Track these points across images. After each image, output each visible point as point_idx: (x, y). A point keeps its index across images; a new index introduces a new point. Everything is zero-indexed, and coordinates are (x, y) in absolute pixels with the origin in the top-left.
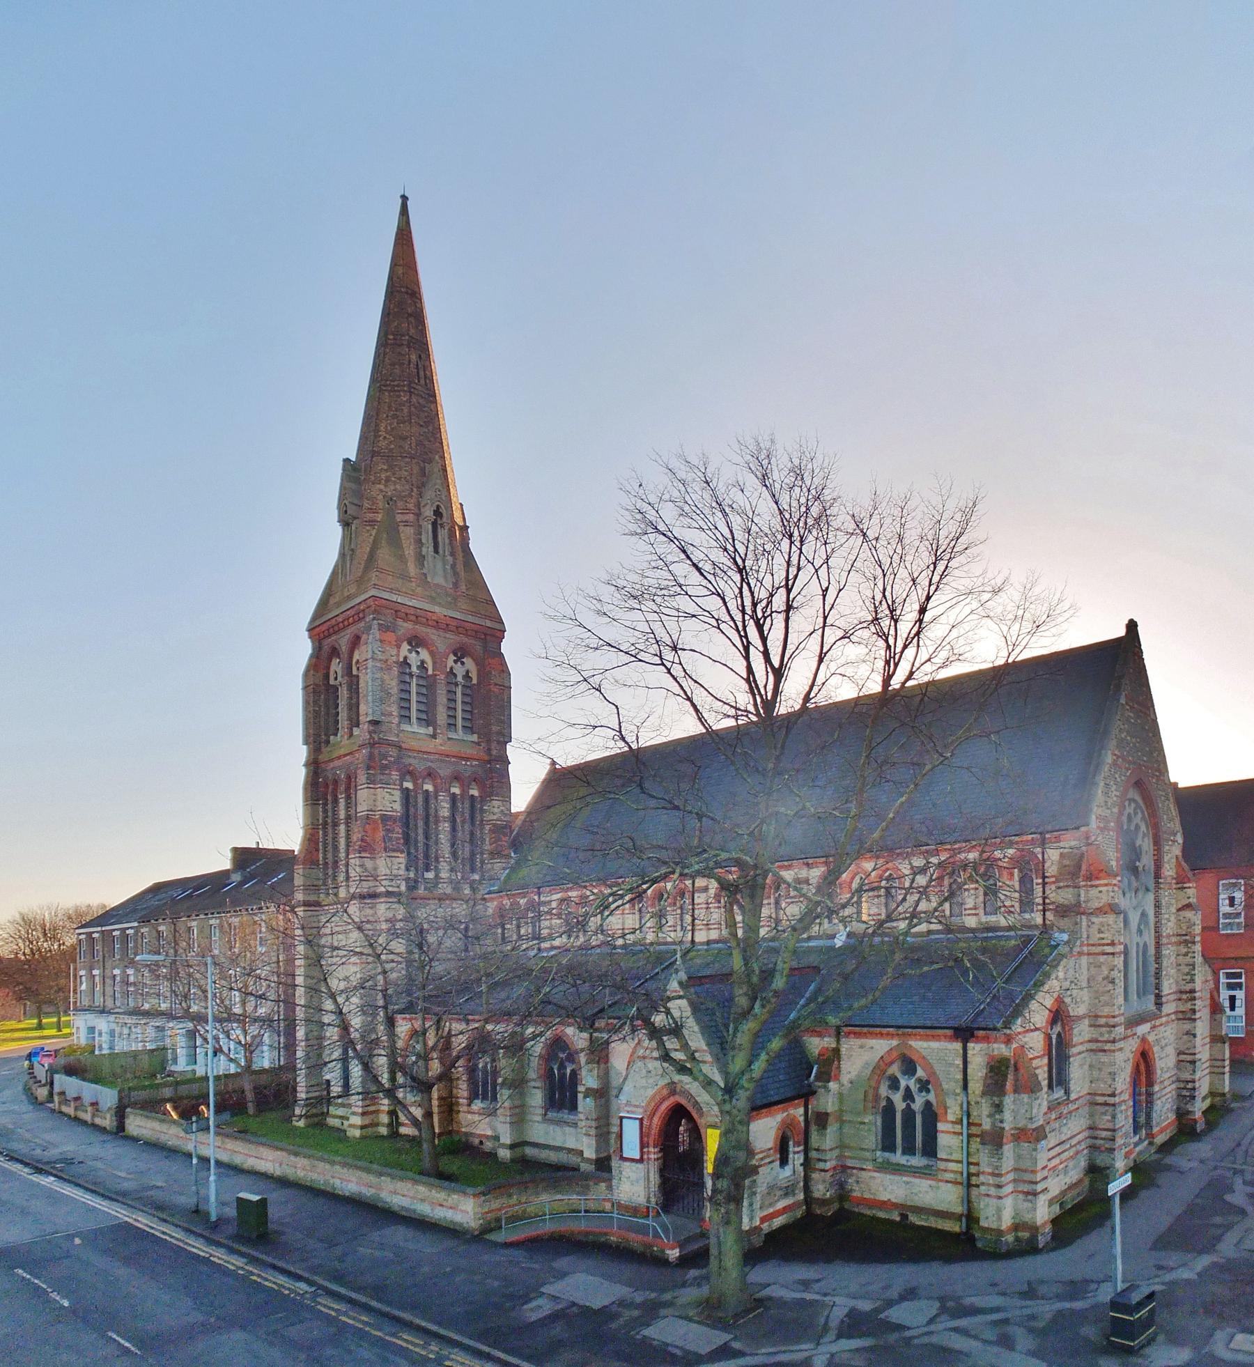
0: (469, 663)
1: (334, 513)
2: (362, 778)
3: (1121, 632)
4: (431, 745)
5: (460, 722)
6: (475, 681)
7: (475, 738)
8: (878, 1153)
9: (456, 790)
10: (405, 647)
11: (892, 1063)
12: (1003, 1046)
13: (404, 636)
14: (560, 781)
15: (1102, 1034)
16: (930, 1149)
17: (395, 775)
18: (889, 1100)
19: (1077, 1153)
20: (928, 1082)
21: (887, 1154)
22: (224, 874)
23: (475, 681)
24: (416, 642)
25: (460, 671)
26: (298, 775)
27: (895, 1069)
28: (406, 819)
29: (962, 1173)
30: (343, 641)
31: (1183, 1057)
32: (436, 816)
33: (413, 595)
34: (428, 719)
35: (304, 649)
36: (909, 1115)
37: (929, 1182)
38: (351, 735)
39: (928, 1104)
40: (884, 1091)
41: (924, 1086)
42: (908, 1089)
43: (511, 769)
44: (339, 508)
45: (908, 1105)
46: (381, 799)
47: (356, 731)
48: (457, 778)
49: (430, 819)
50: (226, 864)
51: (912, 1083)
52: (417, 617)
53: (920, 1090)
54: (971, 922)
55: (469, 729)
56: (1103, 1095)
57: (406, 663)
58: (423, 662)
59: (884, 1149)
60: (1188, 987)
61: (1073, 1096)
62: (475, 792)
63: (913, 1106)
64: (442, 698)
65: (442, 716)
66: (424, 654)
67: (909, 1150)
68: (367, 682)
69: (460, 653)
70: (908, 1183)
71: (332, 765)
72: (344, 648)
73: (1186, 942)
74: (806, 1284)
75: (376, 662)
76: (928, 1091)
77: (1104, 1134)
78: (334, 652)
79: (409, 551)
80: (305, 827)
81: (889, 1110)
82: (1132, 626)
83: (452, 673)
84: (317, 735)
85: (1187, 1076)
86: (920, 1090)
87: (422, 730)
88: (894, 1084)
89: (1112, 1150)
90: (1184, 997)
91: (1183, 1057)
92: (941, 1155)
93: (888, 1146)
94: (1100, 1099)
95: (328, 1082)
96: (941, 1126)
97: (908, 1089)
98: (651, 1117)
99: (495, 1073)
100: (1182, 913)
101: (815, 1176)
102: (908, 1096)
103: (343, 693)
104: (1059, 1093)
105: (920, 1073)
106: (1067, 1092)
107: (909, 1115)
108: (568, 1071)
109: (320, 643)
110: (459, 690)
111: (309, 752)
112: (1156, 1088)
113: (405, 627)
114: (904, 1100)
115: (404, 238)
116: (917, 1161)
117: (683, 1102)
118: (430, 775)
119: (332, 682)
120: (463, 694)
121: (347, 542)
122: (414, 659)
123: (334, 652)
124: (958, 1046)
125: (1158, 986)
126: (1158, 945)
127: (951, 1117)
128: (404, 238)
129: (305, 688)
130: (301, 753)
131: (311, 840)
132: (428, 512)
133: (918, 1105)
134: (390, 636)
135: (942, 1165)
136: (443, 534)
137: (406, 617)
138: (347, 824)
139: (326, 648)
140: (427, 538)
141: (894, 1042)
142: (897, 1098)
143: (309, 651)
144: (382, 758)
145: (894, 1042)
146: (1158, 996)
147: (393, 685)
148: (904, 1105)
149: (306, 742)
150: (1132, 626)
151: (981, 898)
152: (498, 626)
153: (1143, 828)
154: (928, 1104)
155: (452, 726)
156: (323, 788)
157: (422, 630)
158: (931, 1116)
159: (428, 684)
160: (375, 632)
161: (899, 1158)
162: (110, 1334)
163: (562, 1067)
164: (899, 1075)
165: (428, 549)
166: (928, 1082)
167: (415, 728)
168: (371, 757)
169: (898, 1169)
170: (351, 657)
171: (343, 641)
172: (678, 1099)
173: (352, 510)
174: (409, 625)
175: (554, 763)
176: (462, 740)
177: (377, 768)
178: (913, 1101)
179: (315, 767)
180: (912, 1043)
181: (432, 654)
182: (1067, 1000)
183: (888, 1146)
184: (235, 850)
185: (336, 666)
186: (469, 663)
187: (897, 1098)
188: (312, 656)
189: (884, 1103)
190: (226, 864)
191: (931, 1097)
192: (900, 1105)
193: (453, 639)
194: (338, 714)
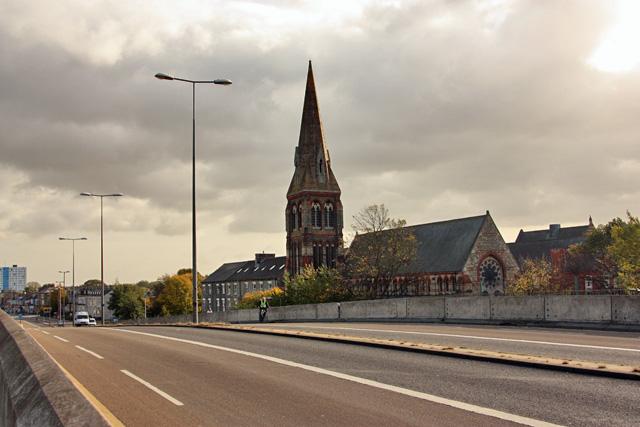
0: (331, 205)
3: (485, 213)
4: (320, 233)
24: (316, 202)
28: (314, 256)
34: (319, 225)
35: (286, 202)
40: (499, 288)
46: (307, 251)
49: (321, 255)
50: (253, 258)
52: (317, 194)
55: (331, 225)
64: (323, 216)
65: (323, 223)
69: (328, 202)
74: (41, 227)
82: (488, 212)
113: (313, 198)
121: (297, 182)
122: (315, 207)
123: (294, 204)
129: (286, 214)
132: (319, 161)
144: (307, 238)
150: (488, 212)
155: (326, 225)
156: (291, 245)
159: (319, 213)
162: (181, 404)
185: (295, 208)
186: (331, 205)
190: (253, 258)
193: (326, 198)
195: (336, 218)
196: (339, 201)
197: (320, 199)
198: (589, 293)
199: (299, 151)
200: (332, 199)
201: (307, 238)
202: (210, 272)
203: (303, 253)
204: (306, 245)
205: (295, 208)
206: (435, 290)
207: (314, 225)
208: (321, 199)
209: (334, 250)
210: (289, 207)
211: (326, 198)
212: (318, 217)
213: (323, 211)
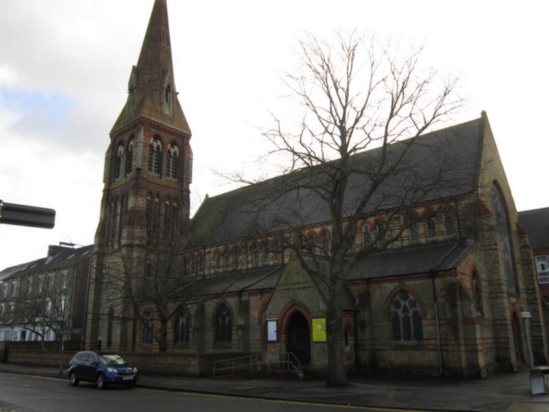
0: (176, 149)
2: (131, 193)
3: (479, 116)
5: (171, 173)
6: (178, 156)
7: (176, 180)
8: (392, 341)
9: (168, 203)
10: (152, 139)
11: (396, 294)
12: (453, 278)
13: (149, 137)
14: (209, 203)
15: (496, 289)
16: (419, 335)
17: (145, 192)
18: (395, 313)
20: (415, 302)
21: (396, 341)
23: (178, 156)
24: (157, 138)
25: (172, 151)
27: (397, 297)
29: (437, 345)
30: (126, 137)
31: (534, 324)
32: (90, 277)
34: (159, 171)
35: (107, 142)
36: (406, 319)
37: (421, 352)
38: (126, 176)
39: (416, 312)
40: (393, 309)
41: (413, 304)
42: (405, 306)
43: (191, 195)
44: (129, 84)
45: (406, 316)
47: (128, 175)
48: (169, 198)
51: (407, 303)
53: (411, 307)
54: (423, 241)
55: (174, 177)
56: (499, 320)
58: (158, 146)
59: (395, 339)
60: (532, 287)
62: (175, 204)
63: (409, 315)
64: (165, 162)
66: (159, 143)
67: (408, 338)
69: (173, 144)
70: (408, 354)
71: (116, 190)
73: (527, 264)
75: (141, 144)
76: (416, 307)
77: (503, 340)
80: (101, 218)
81: (396, 318)
82: (484, 113)
83: (169, 152)
84: (110, 178)
86: (411, 307)
87: (156, 175)
88: (398, 305)
90: (530, 292)
91: (534, 324)
92: (425, 337)
93: (396, 336)
95: (100, 341)
97: (405, 306)
98: (282, 319)
99: (188, 326)
100: (523, 250)
102: (405, 310)
103: (123, 161)
105: (411, 297)
107: (406, 319)
108: (227, 320)
109: (115, 139)
110: (171, 160)
111: (105, 186)
113: (153, 131)
114: (403, 312)
116: (413, 342)
117: (299, 309)
118: (158, 196)
119: (118, 155)
120: (173, 162)
124: (431, 281)
127: (429, 317)
130: (102, 186)
132: (166, 86)
133: (410, 315)
135: (425, 342)
138: (121, 216)
139: (117, 141)
140: (164, 96)
141: (397, 284)
142: (400, 312)
144: (138, 184)
145: (397, 284)
147: (147, 153)
148: (403, 316)
149: (104, 182)
150: (484, 113)
151: (427, 230)
152: (188, 133)
154: (416, 312)
158: (418, 318)
159: (160, 155)
163: (224, 319)
164: (399, 300)
166: (415, 302)
167: (154, 173)
169: (401, 348)
170: (129, 143)
171: (126, 137)
172: (297, 308)
173: (134, 85)
174: (154, 130)
175: (207, 196)
176: (170, 180)
178: (408, 312)
180: (406, 283)
181: (162, 143)
186: (176, 149)
187: (400, 312)
188: (110, 145)
189: (393, 316)
191: (418, 309)
192: (401, 315)
193: (171, 137)
194: (119, 169)
195: (181, 166)
196: (189, 146)
197: (163, 135)
198: (334, 256)
199: (137, 71)
200: (179, 140)
201: (138, 184)
202: (276, 336)
203: (130, 205)
204: (136, 195)
205: (121, 149)
206: (141, 239)
207: (150, 169)
208: (167, 138)
209: (176, 210)
210: (113, 149)
211: (171, 137)
212: (157, 158)
213: (165, 153)
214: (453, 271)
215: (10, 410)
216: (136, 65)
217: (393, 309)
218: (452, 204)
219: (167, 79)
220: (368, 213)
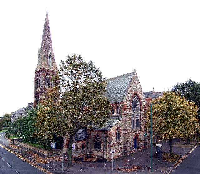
1: (37, 56)
2: (40, 94)
10: (46, 75)
16: (100, 148)
19: (122, 150)
22: (27, 107)
24: (47, 74)
26: (33, 93)
27: (97, 136)
30: (38, 74)
33: (46, 68)
35: (34, 75)
36: (98, 142)
57: (46, 77)
61: (121, 141)
66: (48, 76)
67: (98, 148)
68: (41, 80)
72: (38, 75)
78: (37, 76)
79: (46, 61)
81: (96, 142)
82: (135, 70)
85: (146, 140)
88: (97, 138)
89: (127, 150)
94: (126, 142)
96: (101, 144)
101: (87, 151)
102: (98, 140)
104: (118, 141)
106: (120, 141)
112: (140, 142)
113: (46, 72)
115: (47, 16)
123: (37, 76)
125: (140, 126)
126: (140, 119)
128: (47, 16)
130: (33, 90)
131: (35, 102)
134: (44, 74)
135: (101, 150)
136: (51, 58)
137: (46, 71)
140: (49, 59)
142: (97, 140)
143: (35, 76)
144: (43, 91)
146: (140, 127)
150: (135, 70)
153: (138, 101)
157: (48, 72)
159: (49, 80)
160: (42, 73)
161: (97, 149)
165: (49, 61)
168: (41, 91)
171: (38, 74)
177: (42, 92)
179: (35, 92)
182: (120, 127)
183: (96, 147)
184: (134, 74)
185: (38, 78)
187: (97, 140)
192: (97, 141)
197: (49, 73)
214: (123, 102)
215: (124, 173)
216: (40, 48)
217: (95, 139)
218: (118, 105)
219: (50, 50)
220: (96, 155)
